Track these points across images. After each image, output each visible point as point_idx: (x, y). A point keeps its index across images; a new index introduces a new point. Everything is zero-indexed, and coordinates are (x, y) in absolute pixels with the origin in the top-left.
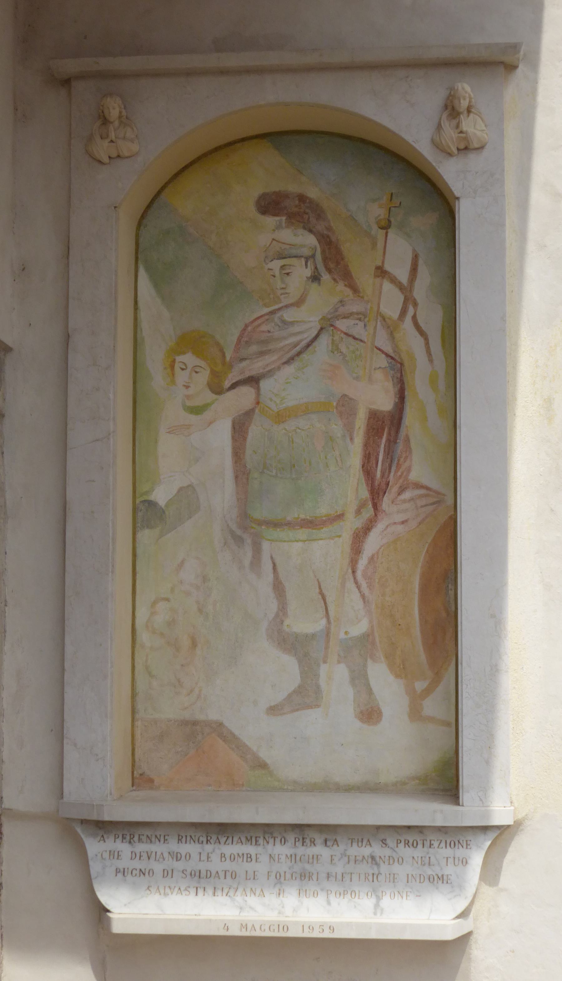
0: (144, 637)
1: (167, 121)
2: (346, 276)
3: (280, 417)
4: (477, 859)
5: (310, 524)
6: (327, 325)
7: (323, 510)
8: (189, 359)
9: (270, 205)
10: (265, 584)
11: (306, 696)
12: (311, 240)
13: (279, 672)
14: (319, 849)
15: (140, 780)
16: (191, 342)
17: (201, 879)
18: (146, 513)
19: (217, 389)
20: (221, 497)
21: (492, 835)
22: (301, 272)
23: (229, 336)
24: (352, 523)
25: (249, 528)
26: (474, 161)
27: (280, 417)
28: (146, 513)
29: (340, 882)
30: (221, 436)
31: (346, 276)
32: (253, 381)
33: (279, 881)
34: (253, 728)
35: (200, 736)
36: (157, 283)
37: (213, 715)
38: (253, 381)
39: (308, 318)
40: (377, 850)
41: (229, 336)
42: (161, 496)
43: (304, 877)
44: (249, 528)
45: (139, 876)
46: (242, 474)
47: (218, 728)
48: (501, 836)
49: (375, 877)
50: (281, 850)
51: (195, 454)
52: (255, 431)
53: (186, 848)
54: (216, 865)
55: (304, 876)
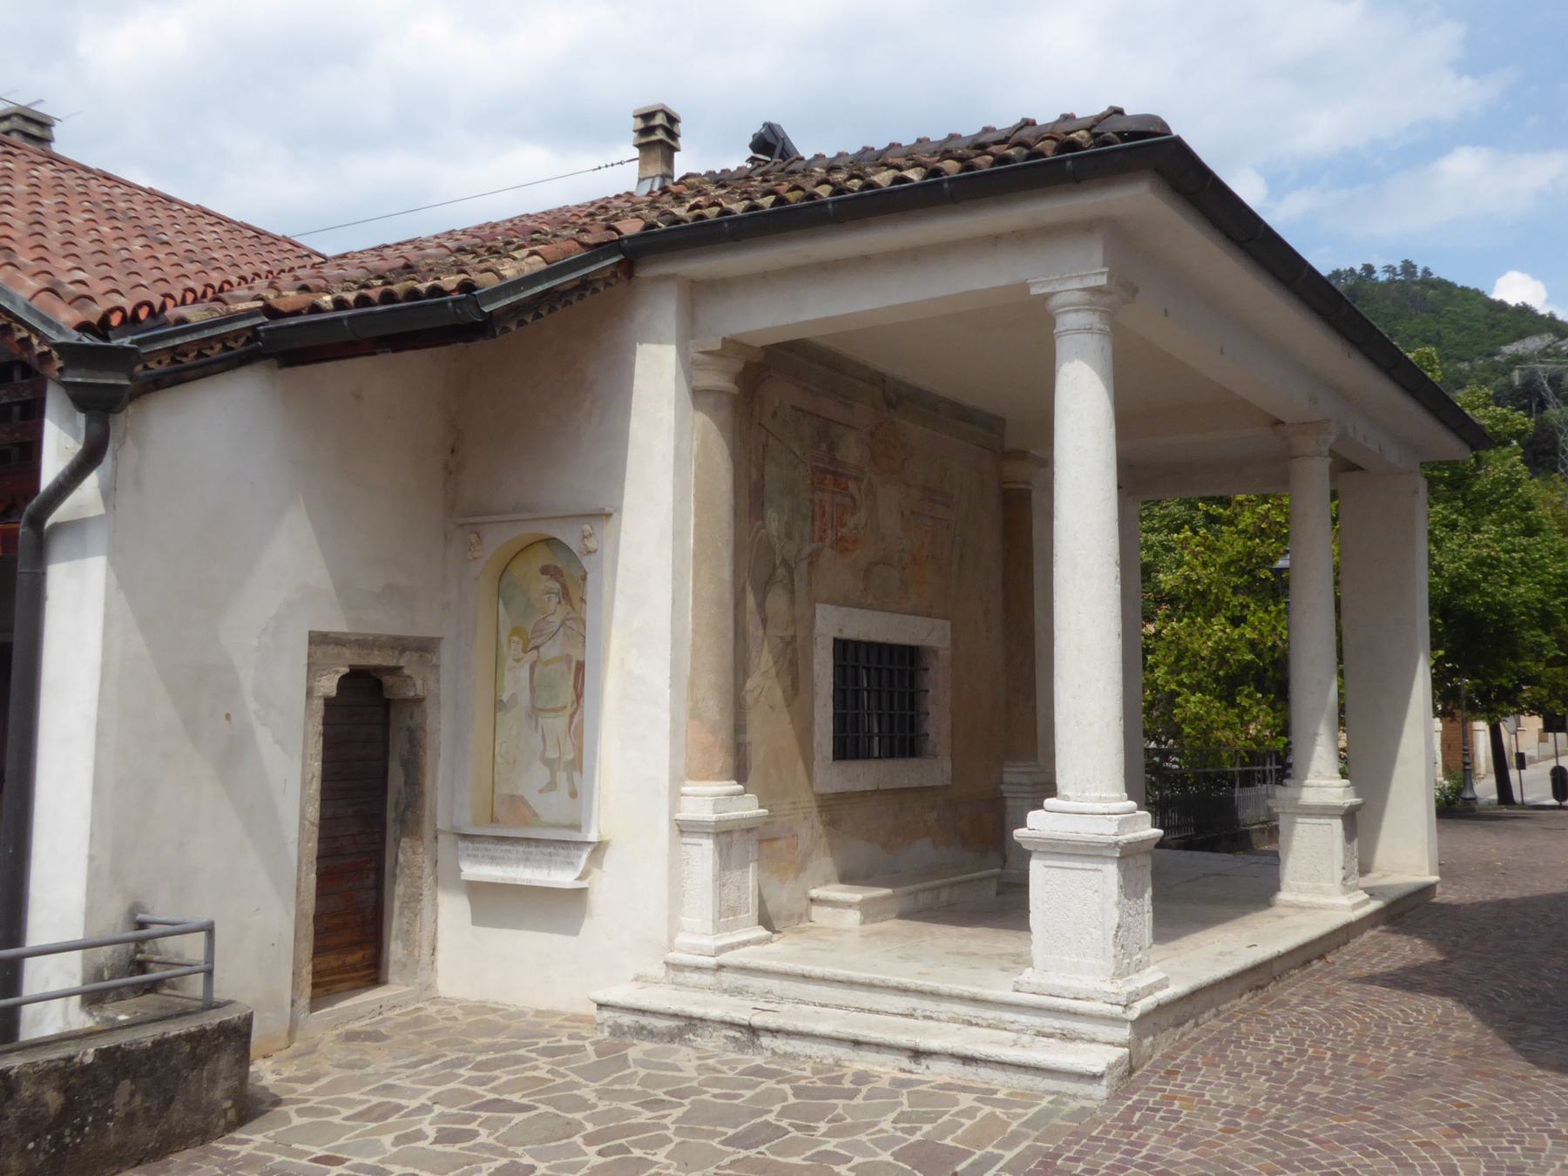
0: (498, 759)
1: (499, 539)
2: (570, 602)
3: (547, 663)
4: (585, 856)
5: (554, 710)
6: (563, 623)
7: (560, 705)
8: (515, 638)
9: (545, 570)
10: (539, 739)
11: (552, 786)
12: (558, 586)
13: (541, 774)
14: (533, 849)
15: (494, 820)
16: (517, 631)
17: (494, 860)
18: (499, 705)
19: (525, 651)
20: (525, 697)
21: (589, 849)
22: (555, 599)
23: (529, 628)
24: (569, 710)
25: (535, 712)
26: (593, 557)
27: (547, 663)
28: (499, 705)
29: (538, 864)
30: (525, 672)
31: (570, 602)
32: (537, 648)
33: (518, 862)
34: (533, 799)
35: (516, 801)
36: (505, 604)
37: (520, 792)
38: (537, 648)
39: (555, 620)
40: (551, 850)
41: (529, 628)
42: (505, 698)
43: (526, 861)
44: (535, 712)
45: (474, 858)
46: (532, 690)
47: (521, 798)
48: (599, 848)
49: (550, 862)
50: (521, 849)
51: (516, 681)
52: (537, 670)
53: (490, 846)
54: (499, 854)
55: (527, 860)
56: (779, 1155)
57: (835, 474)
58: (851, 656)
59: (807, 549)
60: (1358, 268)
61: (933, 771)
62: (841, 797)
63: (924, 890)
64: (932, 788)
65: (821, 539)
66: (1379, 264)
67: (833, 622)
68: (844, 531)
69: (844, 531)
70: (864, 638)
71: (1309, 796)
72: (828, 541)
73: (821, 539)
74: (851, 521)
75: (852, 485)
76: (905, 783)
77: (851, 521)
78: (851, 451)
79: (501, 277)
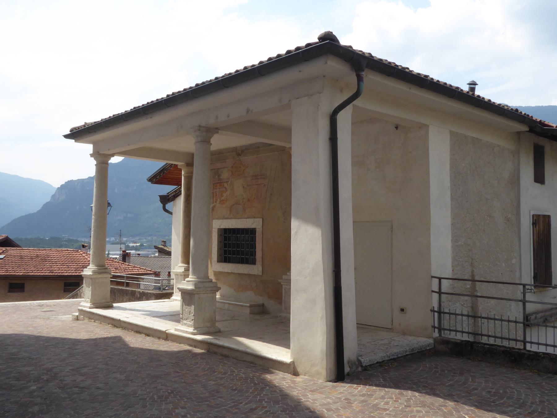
56: (189, 351)
57: (220, 183)
58: (226, 235)
59: (212, 206)
60: (530, 116)
61: (256, 270)
62: (221, 273)
63: (212, 266)
64: (254, 275)
65: (216, 202)
66: (523, 113)
67: (218, 224)
68: (223, 198)
69: (223, 198)
70: (227, 227)
71: (522, 347)
72: (218, 202)
73: (216, 202)
74: (225, 195)
75: (225, 185)
76: (242, 272)
77: (225, 195)
78: (225, 175)
79: (525, 348)
